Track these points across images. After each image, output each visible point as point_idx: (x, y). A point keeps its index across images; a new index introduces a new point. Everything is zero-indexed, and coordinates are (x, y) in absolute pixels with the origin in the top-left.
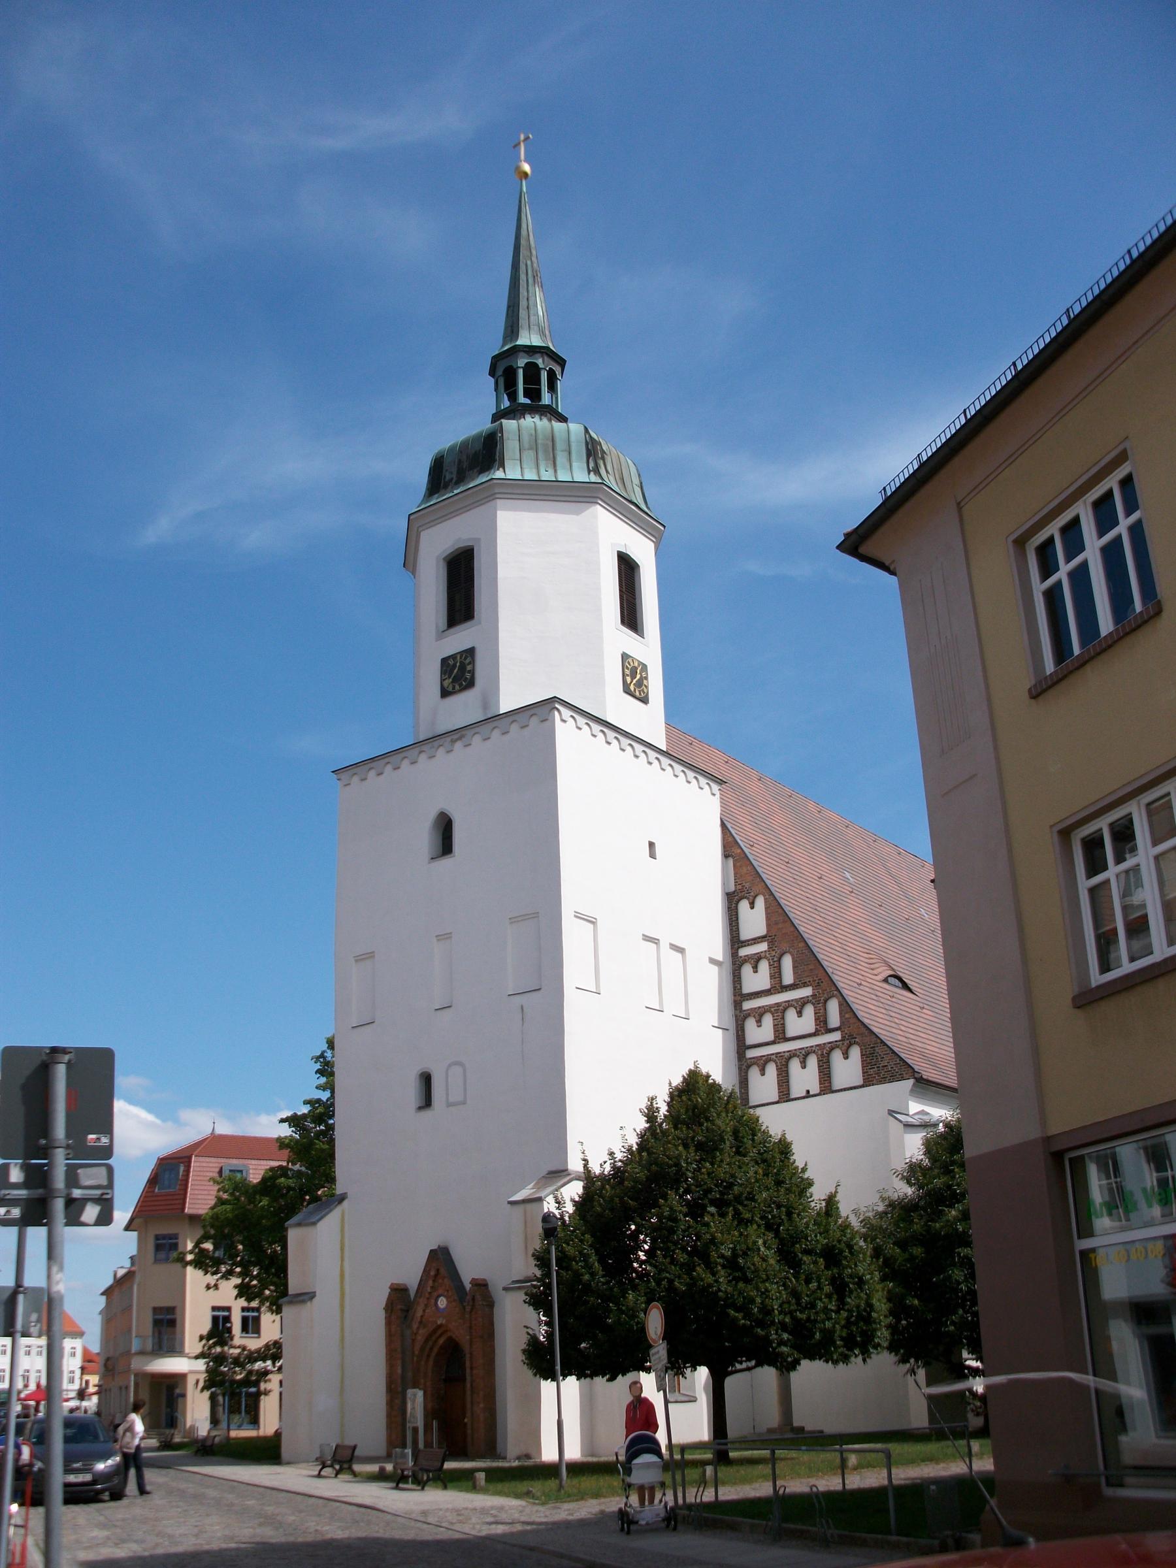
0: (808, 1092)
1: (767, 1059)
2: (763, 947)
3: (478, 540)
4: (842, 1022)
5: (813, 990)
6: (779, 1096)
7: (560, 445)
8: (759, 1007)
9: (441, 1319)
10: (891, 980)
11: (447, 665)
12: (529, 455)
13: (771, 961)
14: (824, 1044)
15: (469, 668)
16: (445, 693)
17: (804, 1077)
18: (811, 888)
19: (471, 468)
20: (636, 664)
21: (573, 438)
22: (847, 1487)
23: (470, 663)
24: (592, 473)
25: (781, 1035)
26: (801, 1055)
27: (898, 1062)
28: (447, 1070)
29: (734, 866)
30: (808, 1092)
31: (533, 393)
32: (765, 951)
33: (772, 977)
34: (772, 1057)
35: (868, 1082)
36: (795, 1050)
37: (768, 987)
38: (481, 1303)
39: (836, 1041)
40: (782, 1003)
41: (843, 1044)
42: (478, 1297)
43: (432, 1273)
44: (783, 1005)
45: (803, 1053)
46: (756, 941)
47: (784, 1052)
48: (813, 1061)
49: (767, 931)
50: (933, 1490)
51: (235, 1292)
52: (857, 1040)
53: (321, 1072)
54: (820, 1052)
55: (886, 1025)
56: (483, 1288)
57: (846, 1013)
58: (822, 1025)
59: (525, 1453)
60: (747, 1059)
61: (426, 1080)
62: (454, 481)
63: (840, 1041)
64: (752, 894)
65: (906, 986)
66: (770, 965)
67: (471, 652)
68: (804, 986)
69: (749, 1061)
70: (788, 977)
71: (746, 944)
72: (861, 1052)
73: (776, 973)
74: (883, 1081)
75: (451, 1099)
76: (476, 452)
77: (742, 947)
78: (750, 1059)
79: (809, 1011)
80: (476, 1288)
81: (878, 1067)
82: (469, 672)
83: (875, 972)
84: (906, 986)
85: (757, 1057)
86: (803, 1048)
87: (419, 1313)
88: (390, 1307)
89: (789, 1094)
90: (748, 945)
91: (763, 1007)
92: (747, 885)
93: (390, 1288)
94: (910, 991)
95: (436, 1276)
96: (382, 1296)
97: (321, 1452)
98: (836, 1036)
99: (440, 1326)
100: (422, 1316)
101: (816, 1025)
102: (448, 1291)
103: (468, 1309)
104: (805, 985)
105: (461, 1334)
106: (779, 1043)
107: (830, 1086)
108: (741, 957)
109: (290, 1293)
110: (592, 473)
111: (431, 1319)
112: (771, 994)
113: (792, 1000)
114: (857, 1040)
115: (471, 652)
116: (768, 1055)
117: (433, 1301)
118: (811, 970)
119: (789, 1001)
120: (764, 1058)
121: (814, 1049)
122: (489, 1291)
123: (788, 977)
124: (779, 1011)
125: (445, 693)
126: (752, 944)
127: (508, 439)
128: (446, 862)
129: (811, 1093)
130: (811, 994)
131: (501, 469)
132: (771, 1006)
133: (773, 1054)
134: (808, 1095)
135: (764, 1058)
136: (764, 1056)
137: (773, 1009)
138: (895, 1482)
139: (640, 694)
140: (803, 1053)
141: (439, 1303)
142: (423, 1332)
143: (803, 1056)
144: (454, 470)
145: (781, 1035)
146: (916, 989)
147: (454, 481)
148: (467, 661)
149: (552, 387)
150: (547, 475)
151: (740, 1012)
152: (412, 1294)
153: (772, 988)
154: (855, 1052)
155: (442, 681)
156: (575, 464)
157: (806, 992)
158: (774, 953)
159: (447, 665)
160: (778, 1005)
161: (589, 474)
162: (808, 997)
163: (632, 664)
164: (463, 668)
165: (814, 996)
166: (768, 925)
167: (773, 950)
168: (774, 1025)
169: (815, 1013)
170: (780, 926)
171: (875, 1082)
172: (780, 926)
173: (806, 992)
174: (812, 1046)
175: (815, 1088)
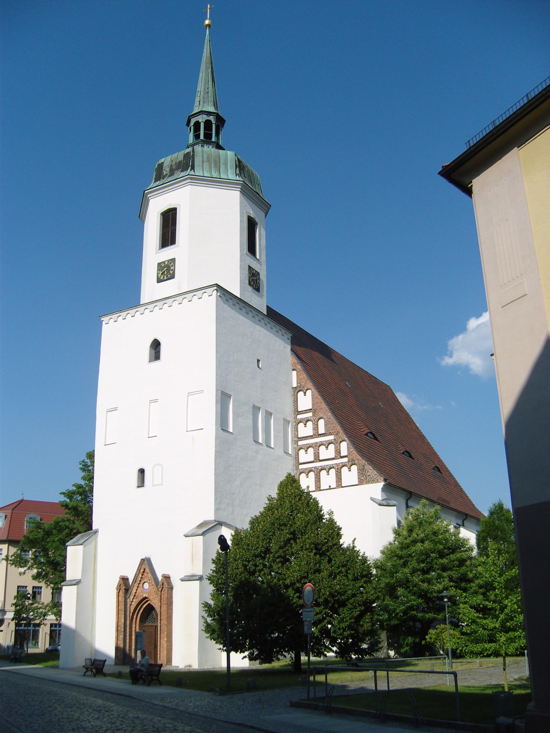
0: (330, 486)
1: (310, 470)
2: (310, 414)
3: (180, 205)
4: (348, 453)
5: (334, 436)
6: (316, 488)
7: (222, 161)
8: (307, 444)
9: (145, 594)
10: (369, 435)
11: (160, 266)
12: (206, 165)
13: (314, 421)
14: (339, 463)
15: (172, 268)
16: (159, 281)
17: (328, 479)
18: (332, 388)
19: (177, 169)
20: (254, 272)
21: (229, 158)
22: (390, 689)
23: (172, 266)
24: (237, 176)
25: (317, 458)
26: (327, 468)
27: (376, 474)
28: (153, 468)
29: (297, 374)
30: (330, 486)
31: (208, 136)
32: (311, 417)
33: (314, 429)
34: (312, 469)
35: (361, 482)
36: (324, 466)
37: (312, 434)
38: (167, 586)
39: (345, 462)
40: (318, 442)
41: (348, 464)
42: (165, 583)
43: (142, 571)
44: (319, 443)
45: (328, 467)
46: (306, 411)
47: (319, 467)
48: (333, 471)
49: (312, 407)
50: (503, 697)
51: (323, 508)
52: (355, 462)
53: (83, 470)
54: (336, 467)
55: (368, 456)
56: (168, 579)
57: (351, 449)
58: (338, 455)
59: (188, 665)
60: (299, 469)
61: (142, 472)
62: (168, 175)
63: (347, 462)
64: (305, 388)
65: (375, 438)
66: (313, 424)
67: (173, 260)
68: (330, 435)
69: (300, 470)
70: (322, 430)
71: (301, 413)
72: (358, 468)
73: (316, 428)
74: (368, 482)
75: (154, 483)
76: (180, 161)
77: (299, 414)
78: (301, 469)
79: (332, 447)
80: (164, 579)
81: (366, 476)
82: (172, 270)
83: (362, 430)
84: (375, 438)
85: (304, 469)
86: (328, 465)
87: (134, 591)
88: (119, 589)
89: (320, 487)
90: (302, 413)
91: (309, 444)
92: (303, 384)
93: (120, 578)
94: (378, 440)
95: (144, 572)
96: (116, 581)
97: (85, 663)
98: (346, 460)
99: (146, 598)
100: (135, 593)
101: (335, 454)
102: (150, 580)
103: (160, 589)
104: (330, 434)
105: (155, 603)
106: (316, 462)
107: (341, 484)
108: (298, 419)
109: (67, 579)
110: (237, 176)
111: (140, 594)
112: (313, 438)
113: (324, 441)
114: (355, 462)
115: (173, 260)
116: (310, 468)
117: (141, 585)
118: (334, 426)
119: (322, 442)
120: (308, 469)
121: (334, 465)
122: (171, 581)
123: (322, 430)
124: (316, 446)
125: (159, 281)
126: (304, 413)
127: (197, 156)
128: (157, 363)
129: (331, 487)
130: (333, 438)
131: (193, 170)
132: (312, 444)
133: (313, 467)
134: (330, 488)
135: (308, 469)
136: (308, 468)
137: (313, 445)
138: (460, 690)
139: (256, 287)
140: (328, 467)
141: (144, 586)
142: (136, 602)
143: (328, 469)
144: (168, 169)
145: (317, 458)
146: (380, 440)
147: (168, 175)
148: (171, 265)
149: (217, 134)
150: (215, 175)
151: (297, 446)
152: (131, 581)
153: (314, 435)
154: (354, 468)
155: (158, 274)
156: (229, 171)
157: (331, 438)
158: (315, 418)
159: (160, 266)
160: (316, 443)
161: (236, 176)
162: (331, 440)
163: (252, 272)
164: (169, 269)
165: (335, 439)
166: (313, 404)
167: (315, 416)
168: (314, 453)
169: (335, 448)
170: (319, 404)
171: (364, 483)
172: (319, 404)
173: (331, 438)
174: (333, 464)
175: (334, 485)
